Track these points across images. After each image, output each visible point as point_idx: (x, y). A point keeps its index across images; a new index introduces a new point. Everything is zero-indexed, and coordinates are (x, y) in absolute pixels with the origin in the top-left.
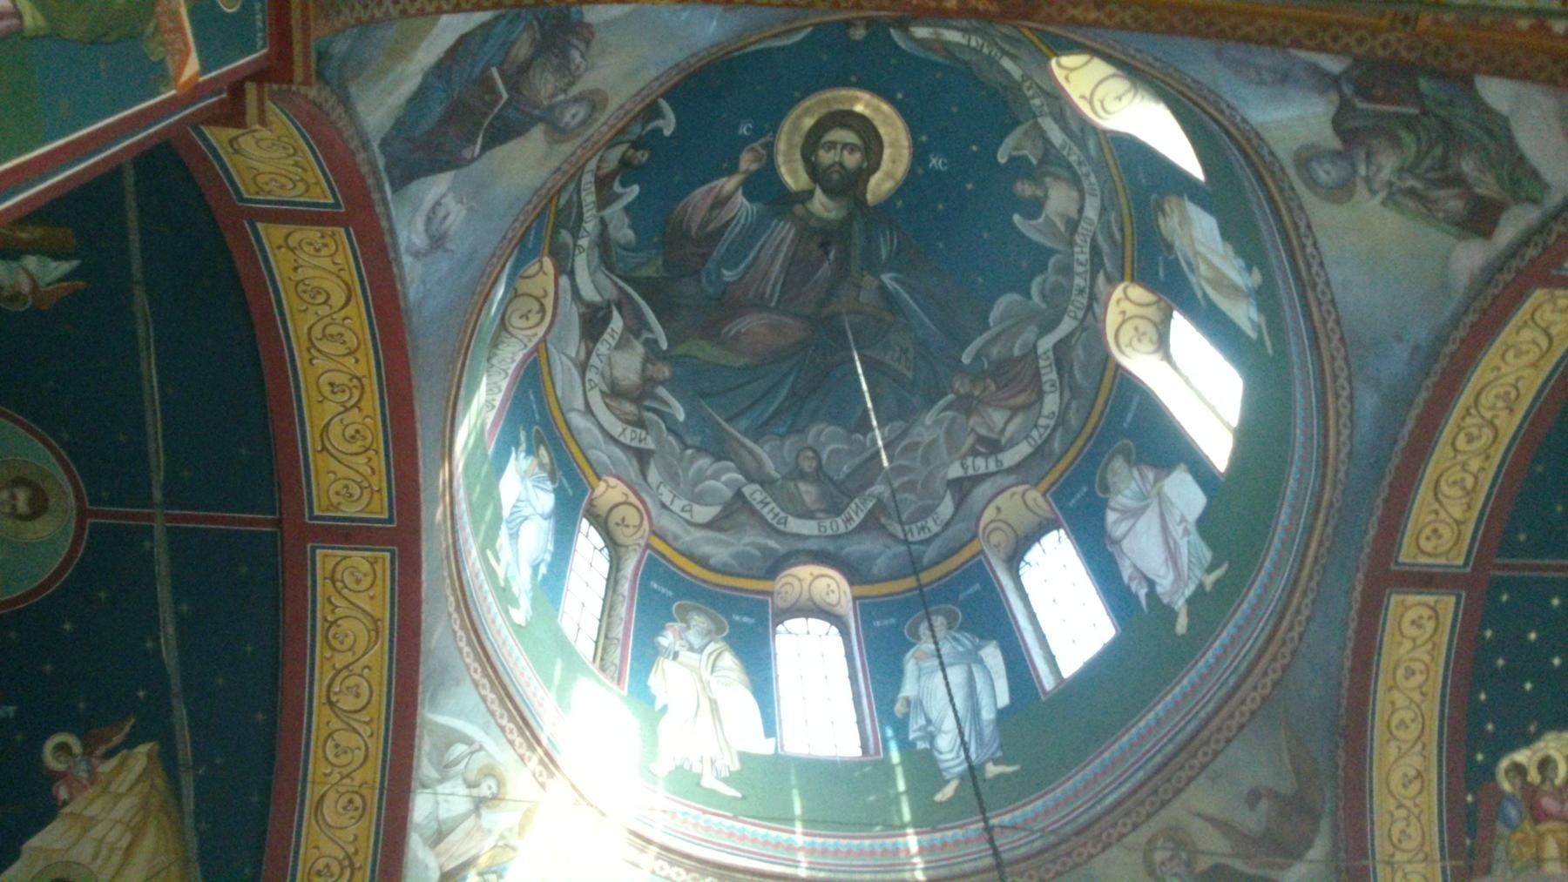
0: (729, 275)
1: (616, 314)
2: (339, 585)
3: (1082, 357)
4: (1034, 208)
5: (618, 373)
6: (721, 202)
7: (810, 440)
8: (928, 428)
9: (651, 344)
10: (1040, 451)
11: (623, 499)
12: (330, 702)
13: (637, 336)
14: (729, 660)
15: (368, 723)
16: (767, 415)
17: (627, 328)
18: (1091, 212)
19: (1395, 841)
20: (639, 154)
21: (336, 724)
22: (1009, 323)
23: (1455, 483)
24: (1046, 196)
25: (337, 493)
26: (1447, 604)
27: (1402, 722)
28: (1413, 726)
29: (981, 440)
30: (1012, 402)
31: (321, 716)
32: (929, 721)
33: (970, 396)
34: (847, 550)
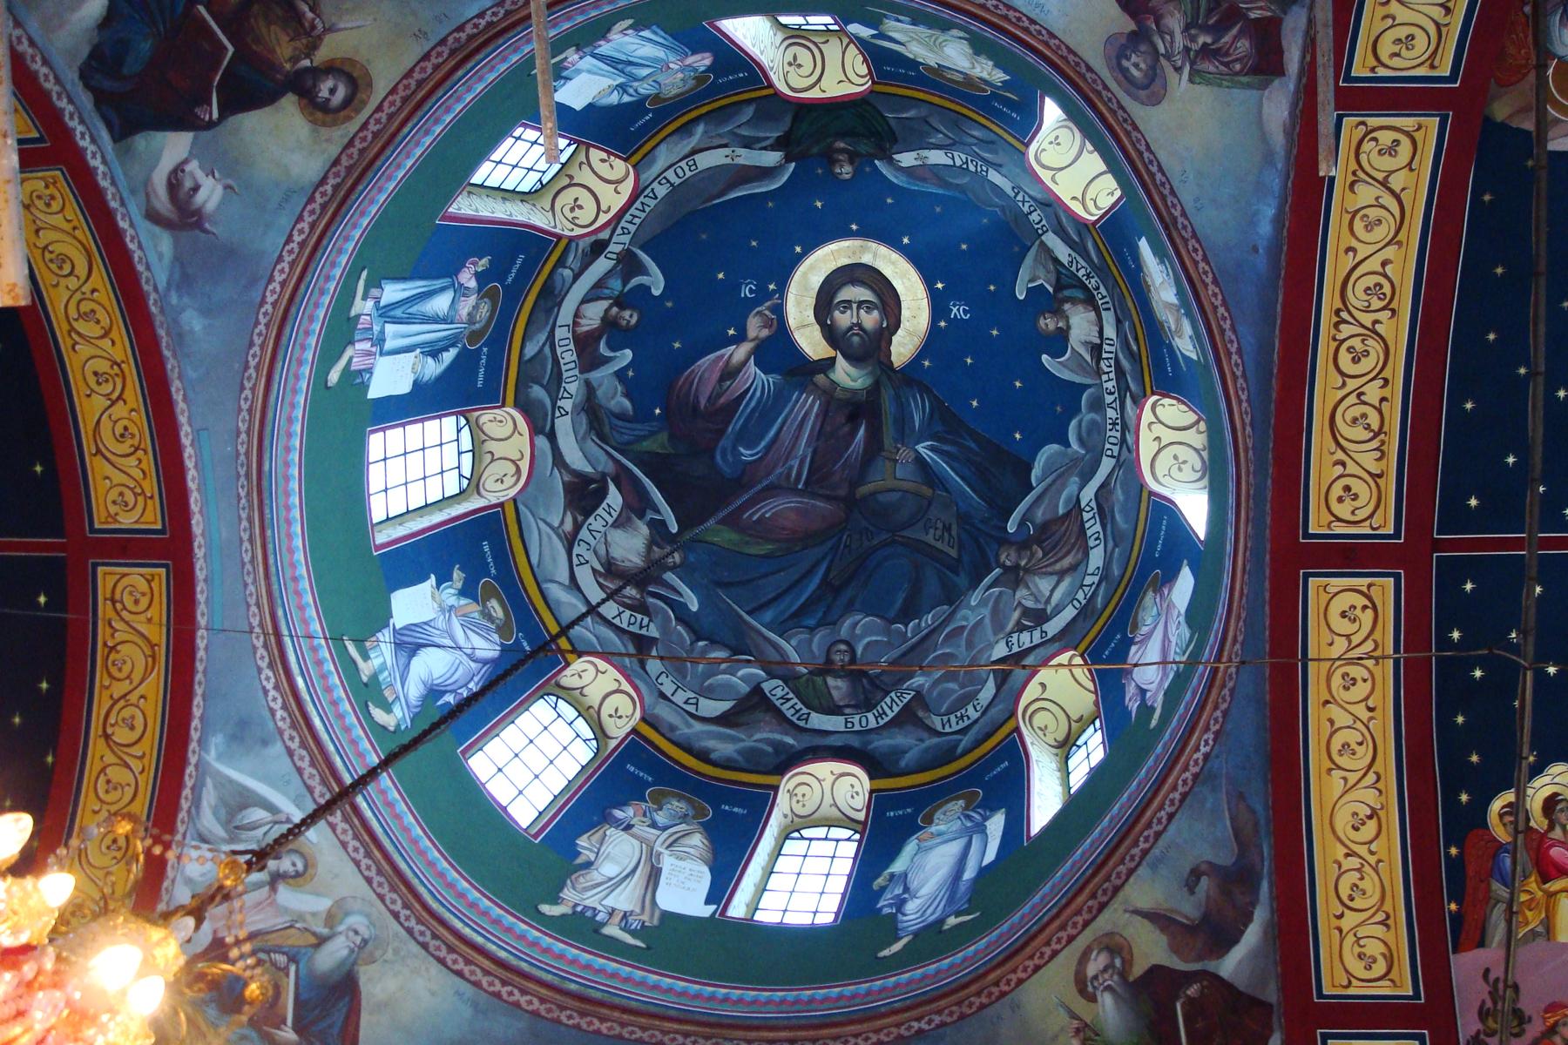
0: (747, 454)
1: (612, 487)
2: (119, 606)
3: (1121, 498)
4: (1058, 343)
5: (617, 553)
6: (730, 373)
7: (844, 631)
8: (972, 609)
9: (658, 527)
10: (1086, 612)
11: (615, 686)
12: (107, 737)
13: (641, 516)
14: (697, 840)
15: (141, 758)
16: (795, 608)
17: (626, 505)
18: (1110, 332)
19: (1344, 894)
20: (626, 314)
21: (110, 758)
22: (1049, 480)
23: (1355, 420)
24: (1069, 327)
25: (114, 502)
26: (1384, 588)
27: (1346, 745)
28: (1360, 750)
29: (1027, 612)
30: (1058, 567)
31: (97, 749)
32: (906, 889)
33: (1017, 567)
34: (876, 744)
